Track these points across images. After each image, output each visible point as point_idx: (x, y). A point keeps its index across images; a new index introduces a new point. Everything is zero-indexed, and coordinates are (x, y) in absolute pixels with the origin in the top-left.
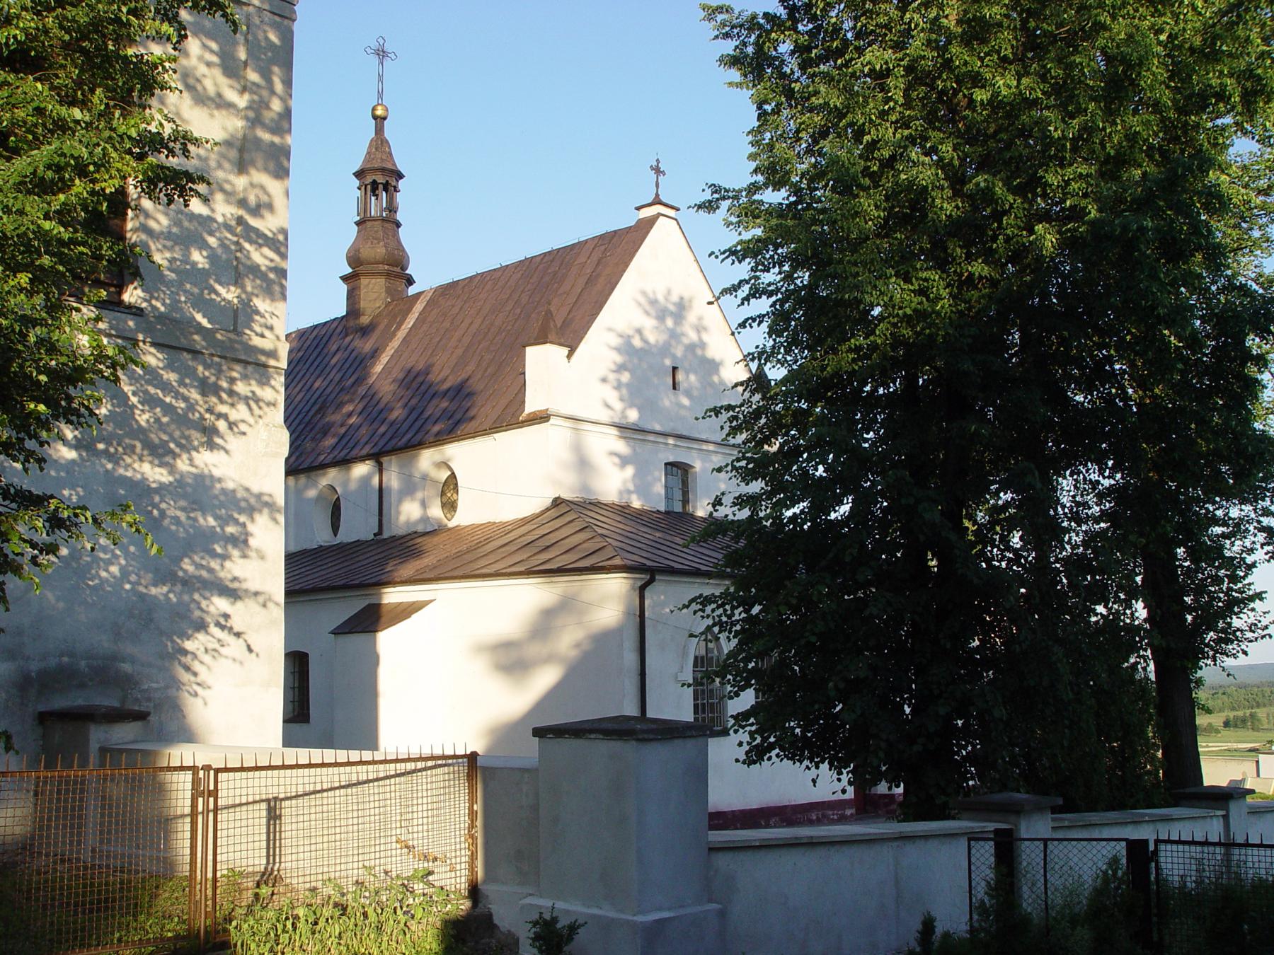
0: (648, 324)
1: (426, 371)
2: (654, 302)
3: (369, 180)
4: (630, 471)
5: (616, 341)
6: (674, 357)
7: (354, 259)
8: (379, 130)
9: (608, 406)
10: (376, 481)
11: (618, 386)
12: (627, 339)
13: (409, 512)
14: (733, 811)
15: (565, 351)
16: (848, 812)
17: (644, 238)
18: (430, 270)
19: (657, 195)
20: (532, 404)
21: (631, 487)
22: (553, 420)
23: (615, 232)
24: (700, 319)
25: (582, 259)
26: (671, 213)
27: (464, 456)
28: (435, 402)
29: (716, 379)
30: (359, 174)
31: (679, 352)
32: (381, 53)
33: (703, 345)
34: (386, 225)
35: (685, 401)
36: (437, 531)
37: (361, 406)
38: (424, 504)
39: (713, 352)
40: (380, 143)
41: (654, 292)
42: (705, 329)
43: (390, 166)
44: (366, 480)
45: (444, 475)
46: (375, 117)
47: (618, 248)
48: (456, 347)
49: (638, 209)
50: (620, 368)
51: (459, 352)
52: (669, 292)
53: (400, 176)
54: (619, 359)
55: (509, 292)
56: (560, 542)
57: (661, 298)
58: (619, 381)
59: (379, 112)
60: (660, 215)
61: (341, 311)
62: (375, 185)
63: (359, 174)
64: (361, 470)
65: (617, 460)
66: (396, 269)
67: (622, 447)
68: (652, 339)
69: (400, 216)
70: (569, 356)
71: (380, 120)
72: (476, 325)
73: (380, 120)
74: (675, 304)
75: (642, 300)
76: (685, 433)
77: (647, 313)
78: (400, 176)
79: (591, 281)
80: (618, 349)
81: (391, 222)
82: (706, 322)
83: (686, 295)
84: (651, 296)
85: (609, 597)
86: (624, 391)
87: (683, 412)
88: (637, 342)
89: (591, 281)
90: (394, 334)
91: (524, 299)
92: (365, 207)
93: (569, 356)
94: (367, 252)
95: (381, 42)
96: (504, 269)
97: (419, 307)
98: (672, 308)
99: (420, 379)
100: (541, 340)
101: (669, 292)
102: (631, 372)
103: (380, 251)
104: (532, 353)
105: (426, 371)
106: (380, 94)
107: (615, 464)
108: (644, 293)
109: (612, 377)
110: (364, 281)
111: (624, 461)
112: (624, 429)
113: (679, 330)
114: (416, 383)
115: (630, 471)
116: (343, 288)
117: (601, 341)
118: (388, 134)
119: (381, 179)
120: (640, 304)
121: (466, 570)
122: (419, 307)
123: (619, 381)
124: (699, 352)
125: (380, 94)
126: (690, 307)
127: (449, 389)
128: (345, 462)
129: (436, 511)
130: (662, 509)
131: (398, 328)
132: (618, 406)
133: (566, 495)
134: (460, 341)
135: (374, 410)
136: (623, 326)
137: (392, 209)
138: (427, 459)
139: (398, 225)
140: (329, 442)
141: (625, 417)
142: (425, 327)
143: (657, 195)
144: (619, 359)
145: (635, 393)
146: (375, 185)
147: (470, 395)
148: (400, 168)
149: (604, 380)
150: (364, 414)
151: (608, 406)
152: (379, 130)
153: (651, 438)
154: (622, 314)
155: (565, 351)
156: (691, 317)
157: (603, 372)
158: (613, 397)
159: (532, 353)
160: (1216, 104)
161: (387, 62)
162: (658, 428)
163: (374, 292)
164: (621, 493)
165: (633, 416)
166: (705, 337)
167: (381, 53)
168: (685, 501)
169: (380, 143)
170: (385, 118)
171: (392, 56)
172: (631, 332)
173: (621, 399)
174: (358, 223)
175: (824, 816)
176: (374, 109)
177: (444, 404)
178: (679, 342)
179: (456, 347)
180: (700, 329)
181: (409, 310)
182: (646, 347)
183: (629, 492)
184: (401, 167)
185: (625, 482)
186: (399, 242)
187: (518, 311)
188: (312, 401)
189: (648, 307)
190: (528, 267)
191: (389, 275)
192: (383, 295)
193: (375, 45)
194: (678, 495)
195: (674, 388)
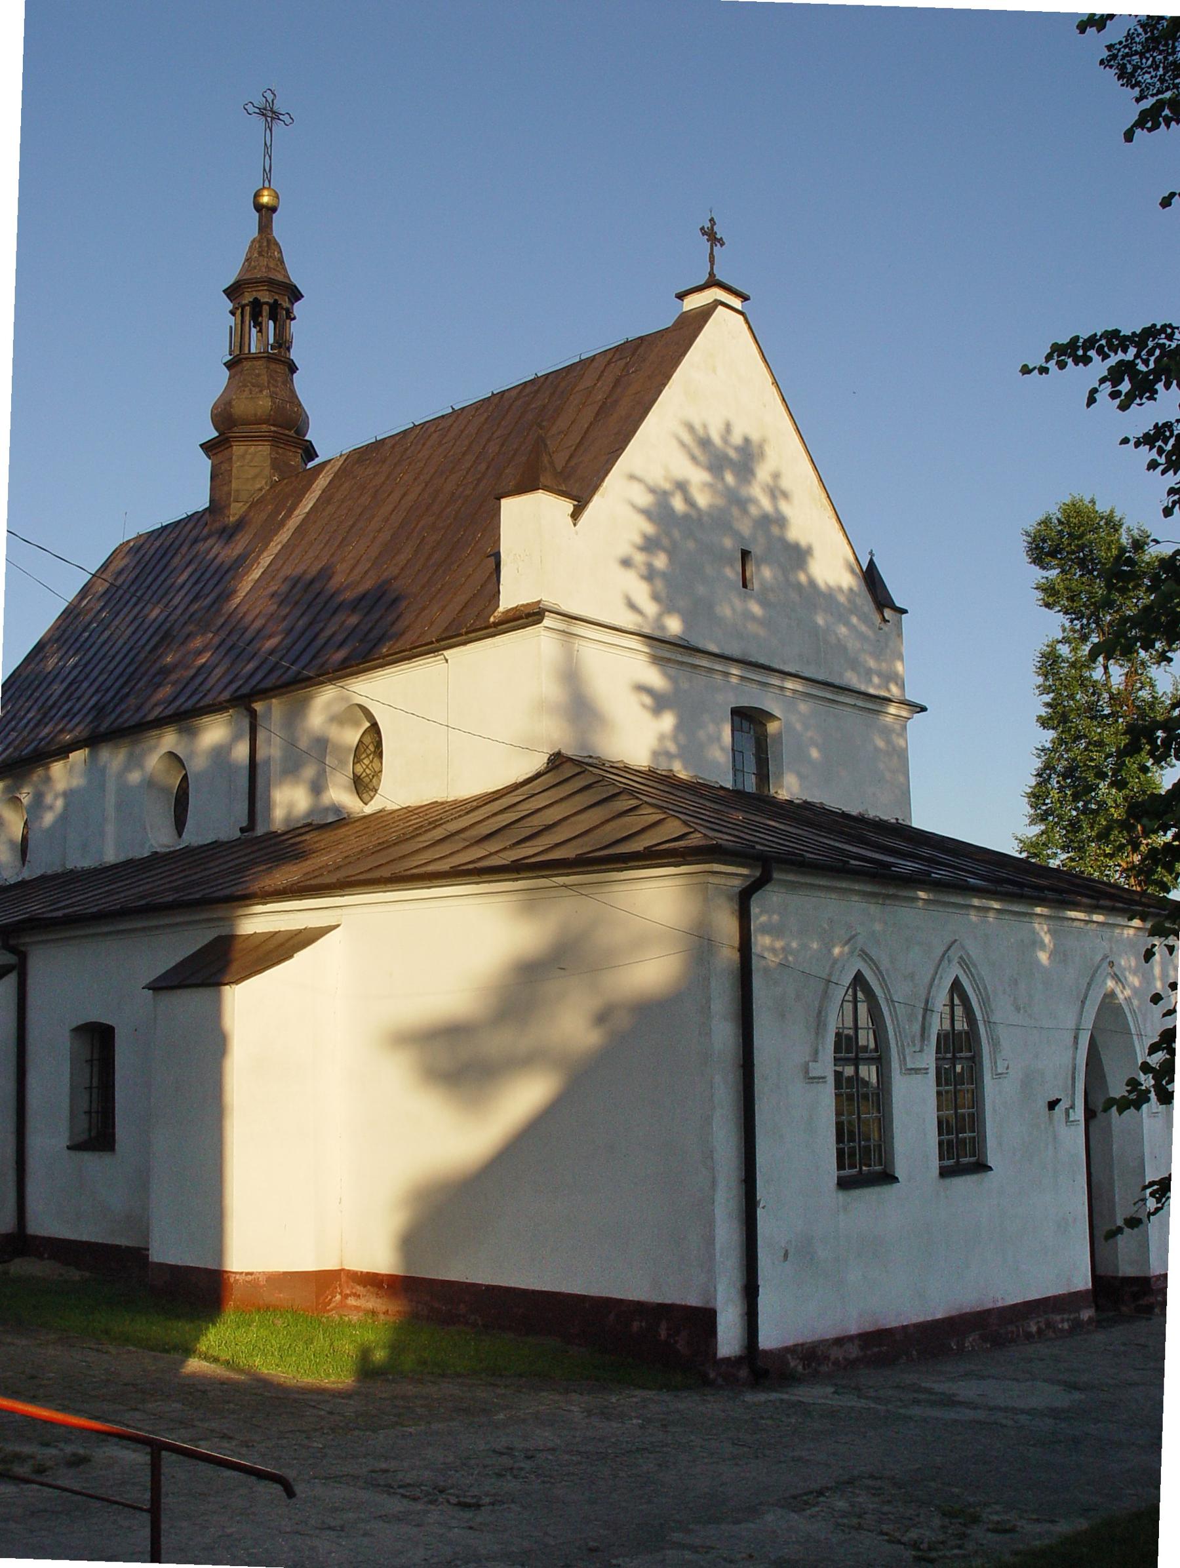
0: (697, 477)
1: (326, 573)
2: (705, 443)
3: (248, 298)
4: (668, 722)
5: (645, 499)
6: (736, 534)
7: (224, 418)
8: (265, 226)
9: (632, 606)
10: (241, 751)
11: (650, 575)
12: (662, 497)
13: (289, 801)
14: (904, 1328)
15: (568, 506)
16: (1086, 1314)
17: (696, 337)
18: (337, 429)
19: (712, 274)
20: (510, 597)
21: (672, 747)
22: (547, 622)
23: (641, 338)
24: (776, 476)
25: (587, 383)
26: (737, 303)
27: (389, 692)
28: (338, 619)
29: (802, 578)
30: (232, 292)
31: (745, 527)
32: (269, 114)
33: (781, 521)
34: (273, 366)
35: (756, 609)
36: (341, 820)
37: (217, 640)
38: (317, 788)
39: (797, 533)
40: (265, 243)
41: (705, 427)
42: (785, 495)
43: (280, 278)
44: (220, 754)
45: (352, 736)
46: (259, 207)
47: (638, 370)
48: (379, 531)
49: (681, 296)
50: (649, 545)
51: (386, 536)
52: (728, 428)
53: (296, 295)
54: (649, 528)
55: (467, 442)
56: (562, 827)
57: (716, 439)
58: (650, 566)
59: (265, 199)
60: (719, 303)
61: (201, 501)
62: (256, 305)
63: (232, 292)
64: (215, 732)
65: (648, 700)
66: (288, 432)
67: (654, 678)
68: (703, 500)
69: (294, 355)
70: (576, 515)
71: (266, 213)
72: (411, 497)
73: (266, 213)
74: (737, 449)
75: (687, 438)
76: (762, 661)
77: (694, 458)
78: (296, 295)
79: (603, 410)
80: (647, 513)
81: (281, 361)
82: (785, 483)
83: (755, 437)
84: (701, 432)
85: (654, 914)
86: (659, 584)
87: (752, 627)
88: (678, 504)
89: (603, 410)
90: (282, 524)
91: (493, 448)
92: (239, 339)
93: (576, 515)
94: (242, 407)
95: (270, 97)
96: (456, 414)
97: (322, 482)
98: (732, 454)
99: (317, 586)
100: (526, 486)
101: (728, 428)
102: (671, 554)
103: (264, 403)
104: (511, 507)
105: (326, 573)
106: (267, 174)
107: (644, 706)
108: (691, 428)
109: (639, 558)
110: (238, 449)
111: (660, 703)
112: (663, 648)
113: (744, 492)
114: (308, 596)
115: (668, 722)
116: (205, 464)
117: (620, 499)
118: (279, 230)
119: (266, 297)
120: (682, 444)
121: (385, 873)
122: (322, 482)
123: (650, 566)
124: (775, 530)
125: (267, 174)
126: (762, 455)
127: (363, 597)
128: (184, 717)
129: (340, 795)
130: (729, 785)
131: (289, 515)
132: (651, 608)
133: (568, 752)
134: (386, 520)
135: (236, 642)
136: (657, 476)
137: (283, 343)
138: (323, 704)
139: (293, 368)
140: (166, 691)
141: (663, 628)
142: (330, 509)
143: (712, 274)
144: (649, 528)
145: (672, 588)
146: (256, 305)
147: (395, 601)
148: (296, 279)
149: (626, 563)
150: (223, 650)
151: (632, 606)
152: (265, 226)
153: (704, 662)
154: (655, 454)
155: (568, 506)
156: (763, 473)
157: (624, 548)
158: (641, 593)
159: (511, 507)
160: (1096, 578)
161: (278, 127)
162: (713, 648)
163: (254, 462)
164: (655, 754)
165: (674, 626)
166: (784, 506)
167: (269, 114)
168: (763, 776)
169: (265, 243)
170: (273, 209)
171: (286, 118)
172: (667, 486)
173: (655, 597)
174: (229, 365)
175: (1049, 1325)
176: (257, 195)
177: (353, 620)
178: (745, 511)
179: (379, 531)
180: (776, 492)
181: (307, 488)
182: (693, 513)
183: (669, 755)
184: (297, 278)
185: (662, 738)
186: (293, 391)
187: (483, 467)
188: (262, 852)
189: (697, 451)
190: (497, 405)
191: (276, 440)
192: (267, 471)
193: (260, 102)
194: (751, 766)
195: (745, 586)
